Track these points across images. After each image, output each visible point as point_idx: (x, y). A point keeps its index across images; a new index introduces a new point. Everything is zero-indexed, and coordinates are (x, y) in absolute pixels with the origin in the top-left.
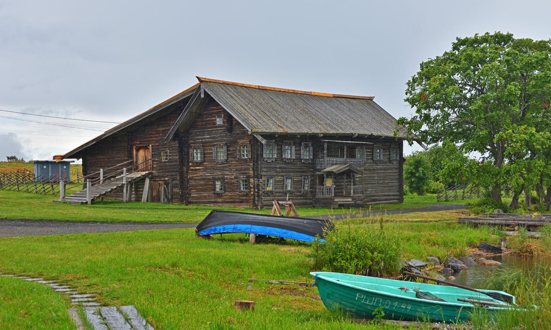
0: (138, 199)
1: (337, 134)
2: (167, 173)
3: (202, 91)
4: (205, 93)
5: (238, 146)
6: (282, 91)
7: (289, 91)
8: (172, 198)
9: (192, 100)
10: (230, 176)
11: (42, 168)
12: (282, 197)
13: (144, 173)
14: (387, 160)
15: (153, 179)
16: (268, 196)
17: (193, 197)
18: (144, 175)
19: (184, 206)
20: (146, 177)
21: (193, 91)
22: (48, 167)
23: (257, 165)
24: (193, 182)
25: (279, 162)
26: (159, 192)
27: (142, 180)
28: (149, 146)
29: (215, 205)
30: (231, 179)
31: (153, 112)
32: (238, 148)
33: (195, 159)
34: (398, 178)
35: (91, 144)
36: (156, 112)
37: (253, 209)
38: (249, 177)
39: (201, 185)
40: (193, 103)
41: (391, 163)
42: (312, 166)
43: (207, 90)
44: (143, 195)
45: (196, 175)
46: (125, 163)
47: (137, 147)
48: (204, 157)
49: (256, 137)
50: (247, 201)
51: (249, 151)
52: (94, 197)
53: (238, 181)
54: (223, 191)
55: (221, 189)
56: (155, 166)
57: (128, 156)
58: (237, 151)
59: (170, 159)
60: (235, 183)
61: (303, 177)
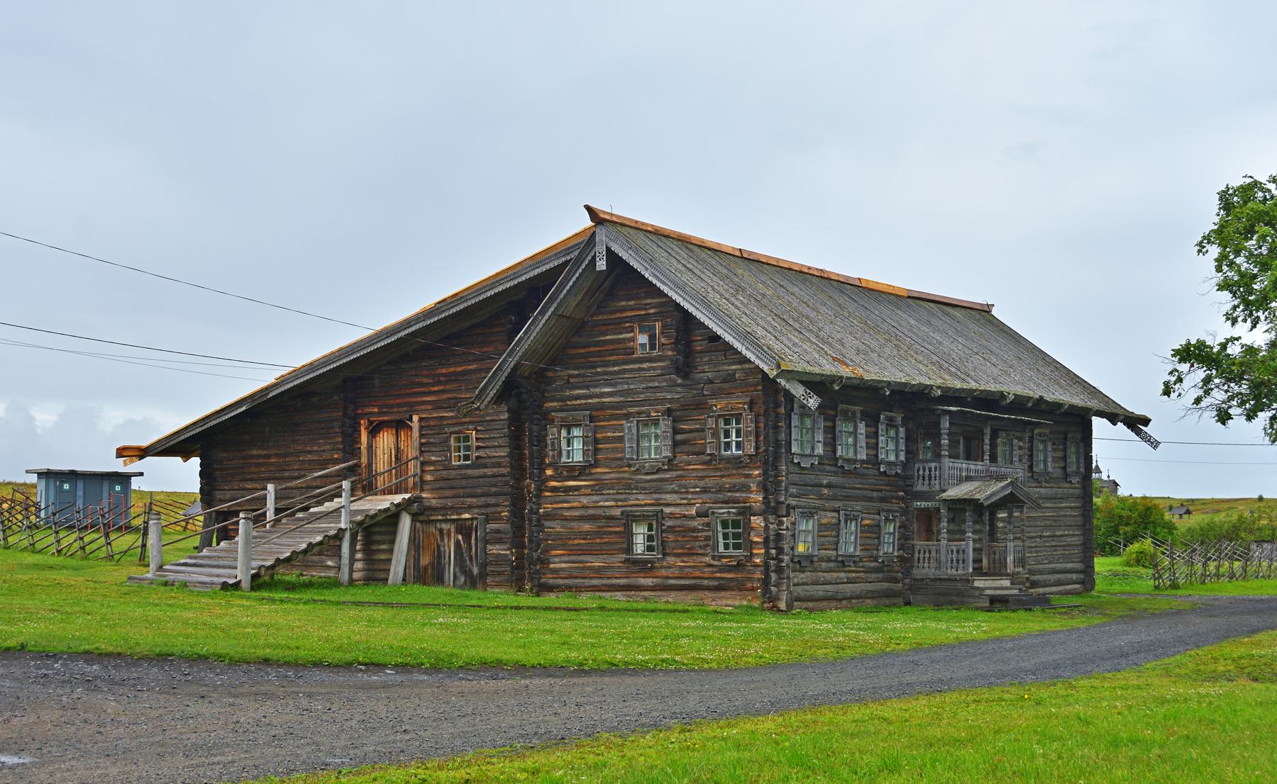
0: (376, 574)
1: (971, 391)
2: (469, 500)
3: (600, 249)
4: (611, 255)
5: (712, 417)
6: (796, 271)
7: (811, 272)
8: (483, 575)
9: (567, 280)
10: (683, 508)
11: (59, 490)
12: (835, 575)
13: (398, 498)
14: (1058, 473)
15: (421, 518)
16: (800, 571)
17: (556, 571)
18: (398, 505)
19: (525, 600)
20: (402, 509)
21: (568, 251)
22: (74, 488)
23: (776, 476)
24: (556, 527)
25: (827, 468)
26: (439, 555)
27: (390, 519)
28: (411, 420)
29: (628, 596)
30: (685, 516)
31: (434, 316)
32: (711, 423)
33: (564, 459)
34: (1079, 523)
35: (229, 416)
36: (443, 316)
37: (763, 610)
38: (747, 512)
39: (584, 536)
40: (568, 287)
41: (1067, 481)
42: (902, 483)
43: (615, 248)
44: (394, 562)
45: (565, 505)
46: (336, 471)
47: (373, 422)
48: (596, 451)
49: (788, 387)
50: (739, 587)
51: (748, 434)
52: (260, 568)
53: (708, 525)
54: (655, 555)
55: (650, 548)
56: (428, 478)
57: (343, 450)
58: (709, 434)
59: (477, 458)
60: (699, 531)
61: (883, 514)
